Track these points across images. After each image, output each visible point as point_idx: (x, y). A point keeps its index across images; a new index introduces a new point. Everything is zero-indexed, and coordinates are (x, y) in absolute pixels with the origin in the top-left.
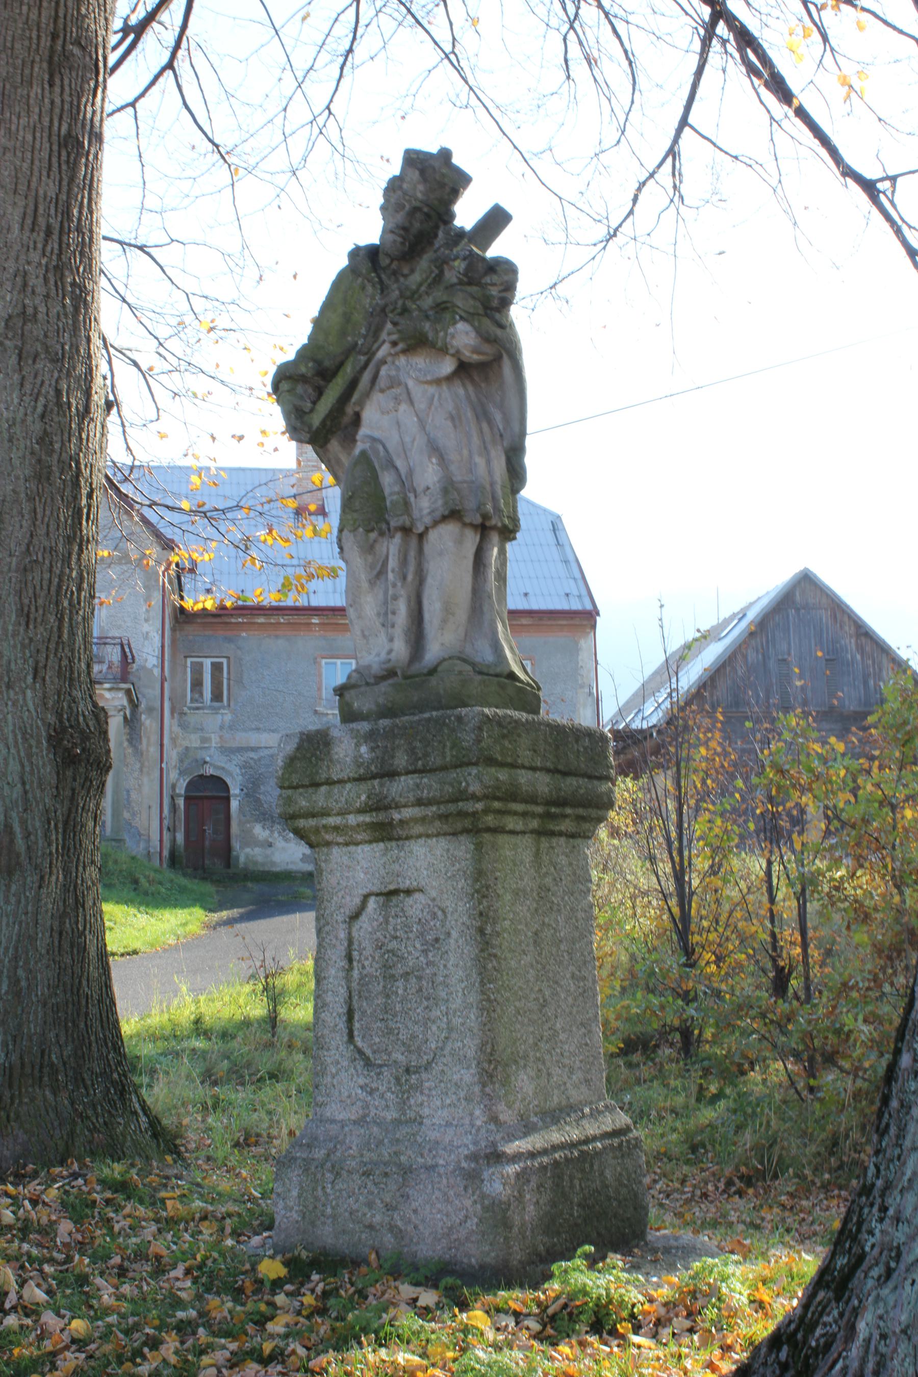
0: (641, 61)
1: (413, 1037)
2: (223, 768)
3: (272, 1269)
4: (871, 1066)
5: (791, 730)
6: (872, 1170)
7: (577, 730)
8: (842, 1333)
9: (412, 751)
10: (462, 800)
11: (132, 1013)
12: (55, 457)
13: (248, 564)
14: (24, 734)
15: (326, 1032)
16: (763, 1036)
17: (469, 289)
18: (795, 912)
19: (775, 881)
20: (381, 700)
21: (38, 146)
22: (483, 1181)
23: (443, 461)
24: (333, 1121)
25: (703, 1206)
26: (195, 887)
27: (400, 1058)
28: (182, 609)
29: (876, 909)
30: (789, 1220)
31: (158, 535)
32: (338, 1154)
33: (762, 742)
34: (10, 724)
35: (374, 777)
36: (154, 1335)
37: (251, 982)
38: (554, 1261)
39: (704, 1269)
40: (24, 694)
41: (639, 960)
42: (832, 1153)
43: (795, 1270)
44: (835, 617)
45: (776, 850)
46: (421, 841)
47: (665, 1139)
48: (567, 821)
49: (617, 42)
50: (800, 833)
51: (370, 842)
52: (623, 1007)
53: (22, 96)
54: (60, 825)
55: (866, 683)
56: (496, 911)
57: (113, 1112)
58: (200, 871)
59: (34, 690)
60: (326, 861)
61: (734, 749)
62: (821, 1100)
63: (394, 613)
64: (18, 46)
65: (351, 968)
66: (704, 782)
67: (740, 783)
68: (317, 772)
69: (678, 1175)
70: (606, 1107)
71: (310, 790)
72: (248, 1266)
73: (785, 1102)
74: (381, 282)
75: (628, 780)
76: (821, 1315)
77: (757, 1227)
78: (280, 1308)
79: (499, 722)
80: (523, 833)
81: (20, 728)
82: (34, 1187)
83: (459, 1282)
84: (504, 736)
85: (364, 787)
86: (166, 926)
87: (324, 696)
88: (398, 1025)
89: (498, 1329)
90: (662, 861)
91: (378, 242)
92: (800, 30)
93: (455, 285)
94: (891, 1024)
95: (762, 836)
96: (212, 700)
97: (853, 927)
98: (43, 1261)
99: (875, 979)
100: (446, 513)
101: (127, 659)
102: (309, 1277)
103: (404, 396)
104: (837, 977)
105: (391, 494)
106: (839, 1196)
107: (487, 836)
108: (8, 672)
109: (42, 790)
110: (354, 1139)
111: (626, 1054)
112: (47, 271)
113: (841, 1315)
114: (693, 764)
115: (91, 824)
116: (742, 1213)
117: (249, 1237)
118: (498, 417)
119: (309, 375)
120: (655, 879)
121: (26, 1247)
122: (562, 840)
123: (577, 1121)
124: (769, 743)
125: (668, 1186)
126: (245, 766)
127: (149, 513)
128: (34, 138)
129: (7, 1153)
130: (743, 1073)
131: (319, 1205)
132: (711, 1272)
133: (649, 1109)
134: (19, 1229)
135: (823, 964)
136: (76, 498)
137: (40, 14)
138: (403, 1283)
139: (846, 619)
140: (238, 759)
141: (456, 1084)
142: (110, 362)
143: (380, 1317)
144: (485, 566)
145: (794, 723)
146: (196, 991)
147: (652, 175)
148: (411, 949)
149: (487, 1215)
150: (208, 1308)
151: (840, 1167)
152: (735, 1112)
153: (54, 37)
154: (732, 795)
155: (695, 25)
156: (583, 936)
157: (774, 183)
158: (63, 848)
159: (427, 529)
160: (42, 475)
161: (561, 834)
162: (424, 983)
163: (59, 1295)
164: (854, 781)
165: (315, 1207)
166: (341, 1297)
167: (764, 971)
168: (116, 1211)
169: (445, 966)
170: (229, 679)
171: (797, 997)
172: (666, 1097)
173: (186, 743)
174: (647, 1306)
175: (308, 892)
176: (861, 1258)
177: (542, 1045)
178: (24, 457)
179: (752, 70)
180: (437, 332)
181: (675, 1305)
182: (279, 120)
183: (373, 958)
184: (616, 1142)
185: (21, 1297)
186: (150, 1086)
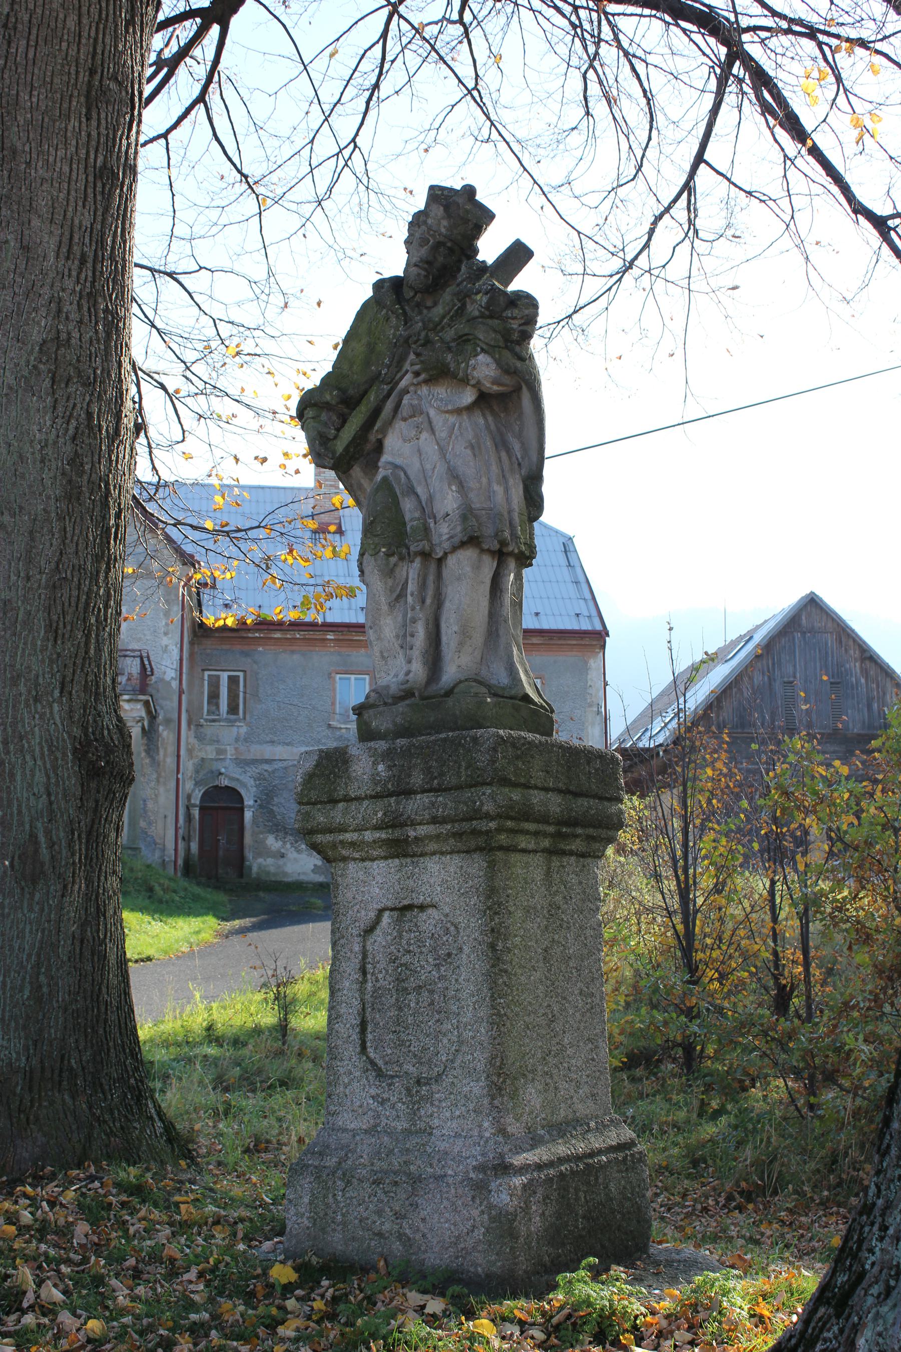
0: (661, 100)
1: (425, 1049)
2: (238, 780)
3: (283, 1273)
4: (871, 1086)
5: (796, 753)
6: (873, 1189)
7: (589, 752)
8: (842, 1348)
9: (428, 771)
10: (476, 819)
11: (146, 1020)
12: (86, 477)
13: (269, 582)
14: (50, 747)
15: (339, 1042)
16: (764, 1053)
17: (490, 322)
18: (798, 931)
19: (778, 901)
20: (399, 720)
21: (74, 177)
22: (490, 1191)
23: (462, 487)
24: (345, 1130)
25: (703, 1220)
26: (209, 896)
27: (412, 1069)
28: (202, 625)
29: (877, 931)
30: (788, 1236)
31: (178, 551)
32: (349, 1162)
33: (767, 763)
34: (37, 737)
35: (390, 795)
36: (168, 1336)
37: (263, 991)
38: (559, 1273)
39: (706, 1283)
40: (51, 707)
41: (643, 975)
42: (831, 1171)
43: (795, 1286)
44: (841, 642)
45: (780, 870)
46: (436, 858)
47: (667, 1153)
48: (578, 841)
49: (636, 82)
50: (805, 854)
51: (385, 858)
52: (627, 1022)
53: (60, 129)
54: (84, 836)
55: (869, 707)
56: (507, 928)
57: (130, 1117)
58: (214, 881)
59: (61, 703)
60: (342, 876)
61: (739, 770)
62: (821, 1118)
63: (412, 636)
64: (57, 80)
65: (365, 981)
66: (709, 802)
67: (745, 804)
68: (335, 789)
69: (679, 1189)
70: (612, 1121)
71: (328, 806)
72: (259, 1271)
73: (785, 1119)
74: (405, 313)
75: (635, 798)
76: (821, 1331)
77: (757, 1242)
78: (291, 1313)
79: (513, 743)
80: (535, 851)
81: (47, 741)
82: (52, 1188)
83: (466, 1291)
84: (518, 757)
85: (380, 804)
86: (180, 934)
87: (338, 711)
88: (410, 1037)
89: (503, 1338)
90: (667, 878)
91: (401, 274)
92: (815, 74)
93: (477, 317)
94: (891, 1044)
95: (766, 856)
96: (228, 713)
97: (855, 947)
98: (60, 1261)
99: (876, 999)
100: (465, 539)
101: (146, 672)
102: (319, 1283)
103: (426, 425)
104: (839, 996)
105: (411, 520)
106: (838, 1213)
107: (500, 855)
108: (36, 686)
109: (67, 802)
110: (365, 1148)
111: (629, 1069)
112: (80, 298)
113: (841, 1331)
114: (700, 784)
115: (113, 835)
116: (742, 1227)
117: (260, 1242)
118: (516, 446)
119: (334, 402)
120: (660, 897)
121: (43, 1247)
122: (573, 858)
123: (583, 1134)
124: (774, 765)
125: (669, 1199)
126: (259, 778)
127: (173, 532)
128: (71, 170)
129: (26, 1155)
130: (745, 1089)
131: (330, 1212)
132: (712, 1286)
133: (652, 1123)
134: (37, 1230)
135: (824, 983)
136: (105, 518)
137: (79, 50)
138: (410, 1291)
139: (851, 643)
140: (253, 770)
141: (465, 1096)
142: (138, 385)
143: (389, 1324)
144: (501, 591)
145: (799, 746)
146: (209, 998)
147: (667, 210)
149: (494, 1225)
150: (220, 1310)
151: (839, 1185)
152: (736, 1127)
153: (92, 72)
154: (737, 815)
155: (711, 64)
156: (591, 954)
157: (787, 218)
158: (86, 858)
159: (446, 554)
160: (72, 495)
161: (571, 853)
163: (75, 1295)
164: (858, 804)
165: (326, 1214)
166: (351, 1303)
167: (766, 989)
168: (131, 1214)
169: (457, 980)
170: (245, 693)
171: (799, 1017)
172: (668, 1111)
173: (202, 755)
174: (649, 1318)
175: (319, 902)
176: (861, 1275)
177: (550, 1059)
178: (55, 477)
179: (766, 109)
180: (459, 364)
181: (677, 1318)
182: (306, 152)
183: (387, 971)
184: (620, 1156)
185: (38, 1297)
186: (162, 1091)
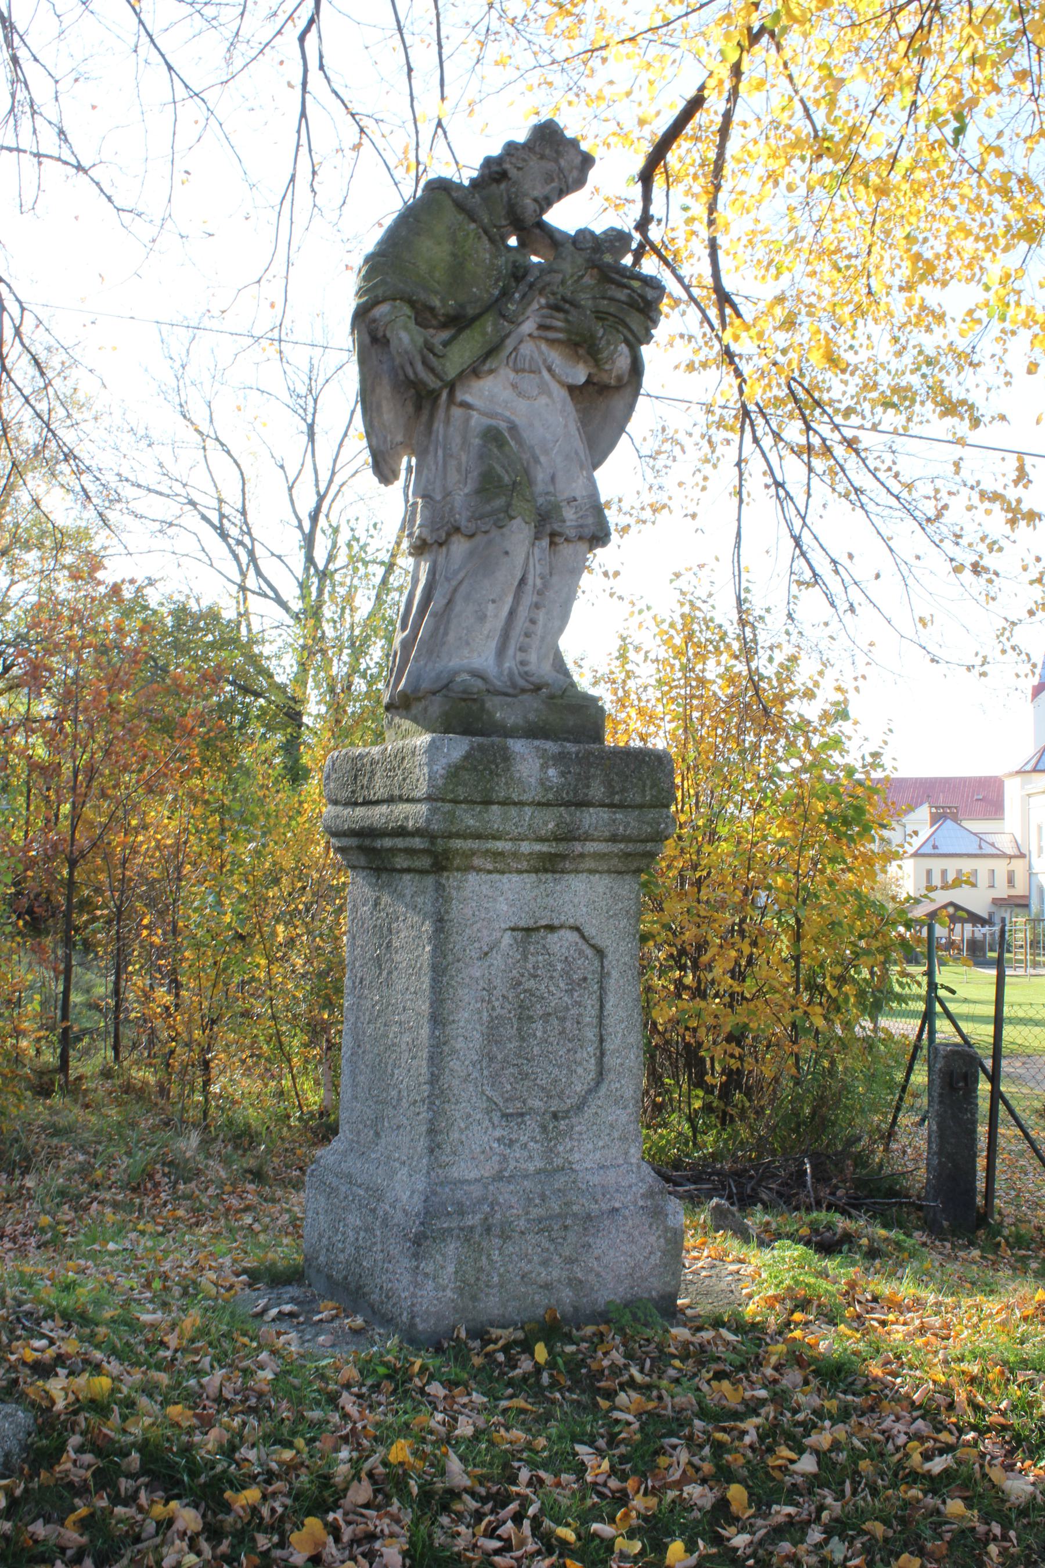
9: (609, 785)
20: (531, 716)
32: (498, 1216)
46: (583, 876)
148: (552, 989)
162: (568, 1024)
